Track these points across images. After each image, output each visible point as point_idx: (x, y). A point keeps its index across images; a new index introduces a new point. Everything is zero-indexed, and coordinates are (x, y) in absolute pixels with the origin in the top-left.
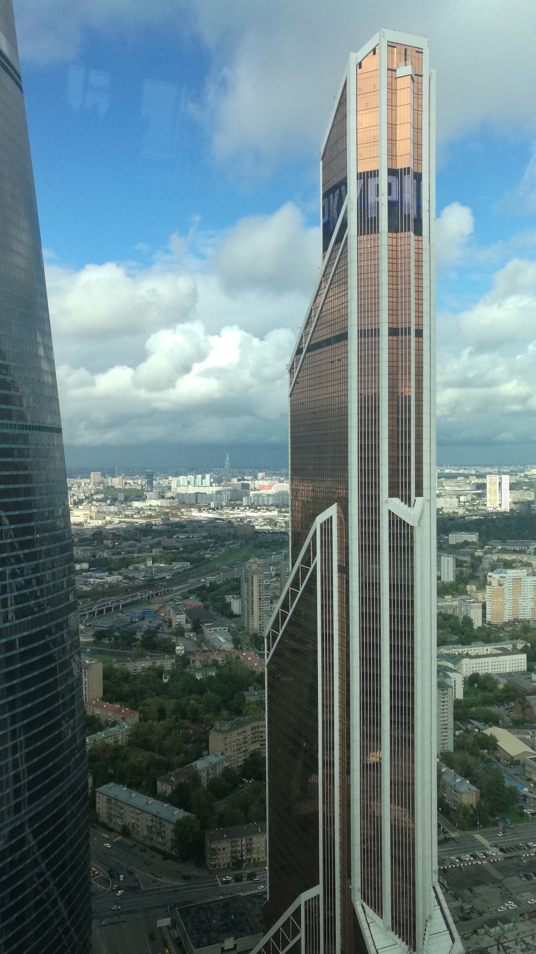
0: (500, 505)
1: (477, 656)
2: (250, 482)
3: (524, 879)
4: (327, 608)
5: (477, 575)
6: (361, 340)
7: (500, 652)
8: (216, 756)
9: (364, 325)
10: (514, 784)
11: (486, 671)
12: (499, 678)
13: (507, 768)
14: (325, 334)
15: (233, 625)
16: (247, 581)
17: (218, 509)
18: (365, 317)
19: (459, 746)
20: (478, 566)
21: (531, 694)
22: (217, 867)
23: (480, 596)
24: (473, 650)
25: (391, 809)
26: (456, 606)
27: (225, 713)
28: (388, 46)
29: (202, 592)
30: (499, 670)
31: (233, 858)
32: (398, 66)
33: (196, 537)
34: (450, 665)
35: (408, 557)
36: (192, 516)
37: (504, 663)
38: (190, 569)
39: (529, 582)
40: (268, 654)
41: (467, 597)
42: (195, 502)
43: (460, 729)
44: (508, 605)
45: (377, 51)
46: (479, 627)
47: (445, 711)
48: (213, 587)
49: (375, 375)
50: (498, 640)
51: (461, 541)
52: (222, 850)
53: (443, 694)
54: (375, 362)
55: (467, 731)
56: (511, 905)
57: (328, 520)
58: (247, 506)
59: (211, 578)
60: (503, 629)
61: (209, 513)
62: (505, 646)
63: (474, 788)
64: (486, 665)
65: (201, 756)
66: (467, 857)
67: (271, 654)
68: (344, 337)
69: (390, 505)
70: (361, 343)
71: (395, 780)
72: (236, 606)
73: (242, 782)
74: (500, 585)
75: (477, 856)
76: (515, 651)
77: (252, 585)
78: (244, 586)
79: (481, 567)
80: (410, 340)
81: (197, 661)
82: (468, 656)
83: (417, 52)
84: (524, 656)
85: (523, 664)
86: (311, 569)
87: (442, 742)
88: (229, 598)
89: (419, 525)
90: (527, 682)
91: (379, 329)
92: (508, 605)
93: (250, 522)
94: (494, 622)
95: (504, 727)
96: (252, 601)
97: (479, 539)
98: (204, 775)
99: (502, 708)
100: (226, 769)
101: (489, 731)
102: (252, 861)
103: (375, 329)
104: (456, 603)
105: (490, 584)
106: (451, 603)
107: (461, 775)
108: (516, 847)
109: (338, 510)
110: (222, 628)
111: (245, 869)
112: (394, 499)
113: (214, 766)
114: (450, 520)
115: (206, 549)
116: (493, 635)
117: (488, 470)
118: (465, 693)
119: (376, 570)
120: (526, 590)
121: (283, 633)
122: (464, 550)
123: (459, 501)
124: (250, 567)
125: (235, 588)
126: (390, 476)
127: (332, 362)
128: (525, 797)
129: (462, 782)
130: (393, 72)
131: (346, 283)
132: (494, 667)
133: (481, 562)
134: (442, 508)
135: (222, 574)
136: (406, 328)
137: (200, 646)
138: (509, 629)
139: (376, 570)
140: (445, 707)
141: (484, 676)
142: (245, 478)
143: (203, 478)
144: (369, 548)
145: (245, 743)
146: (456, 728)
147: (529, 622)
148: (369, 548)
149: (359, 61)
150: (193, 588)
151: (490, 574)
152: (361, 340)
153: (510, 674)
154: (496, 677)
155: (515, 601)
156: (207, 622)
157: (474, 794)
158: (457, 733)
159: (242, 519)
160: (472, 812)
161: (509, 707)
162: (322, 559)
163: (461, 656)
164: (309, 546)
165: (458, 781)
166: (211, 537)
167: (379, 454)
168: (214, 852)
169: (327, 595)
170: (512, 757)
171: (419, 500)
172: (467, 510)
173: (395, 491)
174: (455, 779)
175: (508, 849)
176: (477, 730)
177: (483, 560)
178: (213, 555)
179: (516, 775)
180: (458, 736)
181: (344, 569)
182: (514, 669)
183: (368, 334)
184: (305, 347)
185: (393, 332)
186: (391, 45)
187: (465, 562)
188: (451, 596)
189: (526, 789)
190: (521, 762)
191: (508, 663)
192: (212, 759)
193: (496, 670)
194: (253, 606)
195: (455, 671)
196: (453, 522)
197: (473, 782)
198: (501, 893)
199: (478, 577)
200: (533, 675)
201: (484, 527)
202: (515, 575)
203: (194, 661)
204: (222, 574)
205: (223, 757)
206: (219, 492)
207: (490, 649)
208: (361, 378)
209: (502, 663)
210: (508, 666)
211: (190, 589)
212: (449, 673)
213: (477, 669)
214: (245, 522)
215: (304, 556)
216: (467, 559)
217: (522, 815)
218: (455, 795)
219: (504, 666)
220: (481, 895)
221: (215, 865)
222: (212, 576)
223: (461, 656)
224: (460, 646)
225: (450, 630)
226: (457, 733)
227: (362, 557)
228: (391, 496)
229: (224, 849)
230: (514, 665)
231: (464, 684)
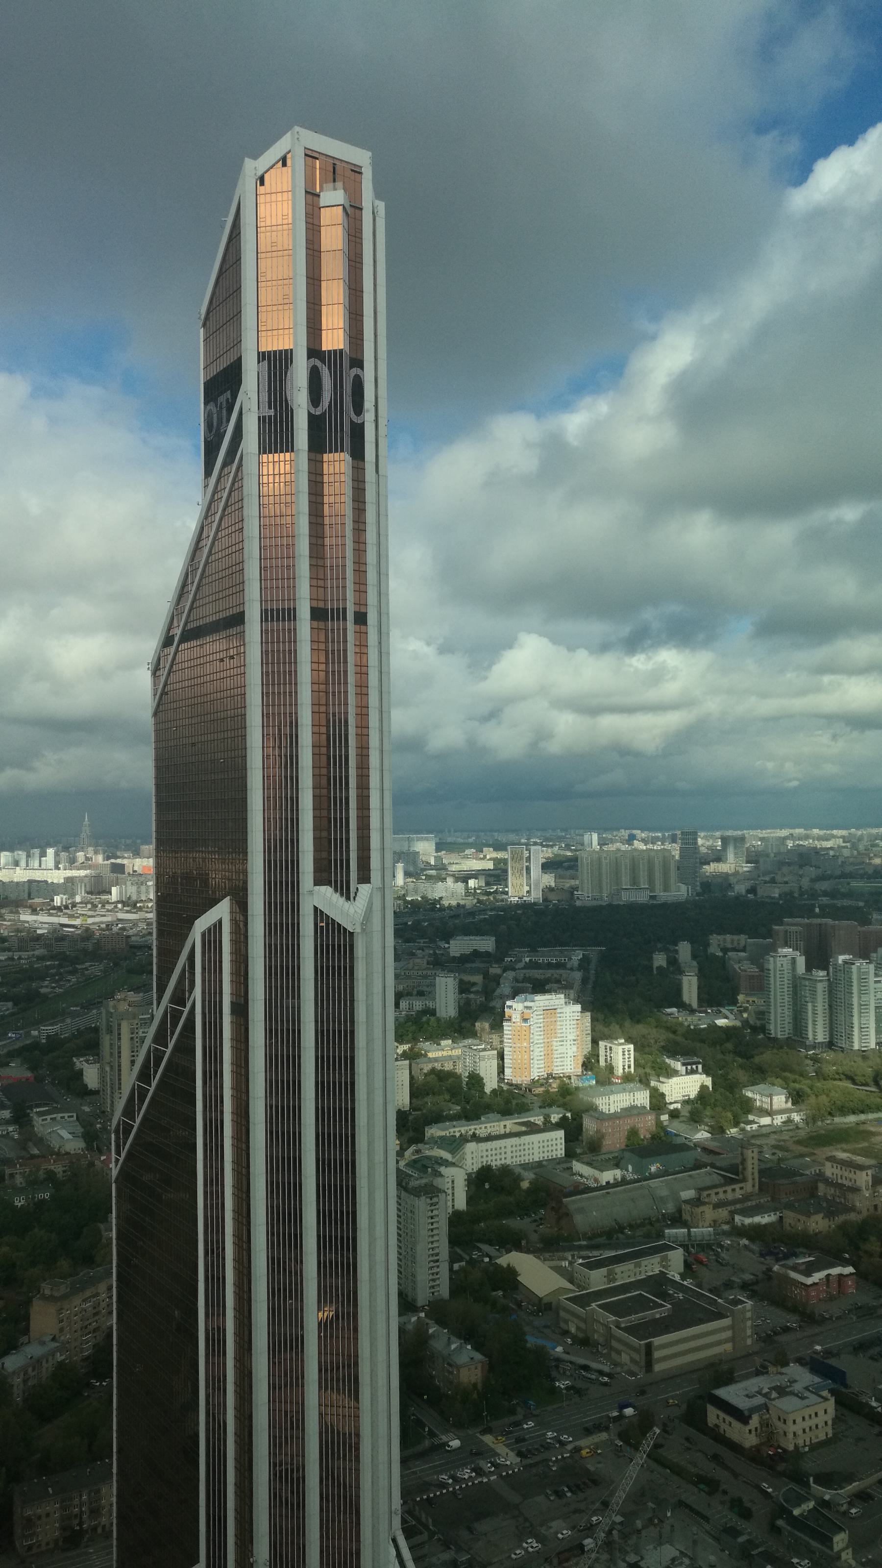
0: (528, 892)
1: (489, 1138)
2: (125, 862)
3: (552, 1498)
4: (213, 1075)
5: (492, 1004)
6: (267, 626)
7: (524, 1129)
8: (43, 1343)
9: (272, 601)
10: (540, 1342)
11: (503, 1162)
12: (522, 1172)
13: (531, 1318)
14: (209, 613)
15: (86, 1109)
16: (110, 1031)
17: (66, 907)
18: (283, 587)
19: (458, 1287)
20: (494, 991)
21: (571, 1194)
22: (35, 1550)
23: (495, 1038)
24: (483, 1128)
25: (320, 1414)
26: (458, 1057)
27: (64, 1264)
28: (306, 155)
29: (30, 1053)
30: (522, 1158)
31: (63, 1529)
32: (321, 189)
33: (24, 957)
34: (446, 1155)
36: (19, 921)
38: (13, 1014)
39: (568, 1015)
40: (117, 1161)
41: (477, 1041)
42: (26, 896)
43: (460, 1259)
44: (538, 1052)
45: (289, 162)
46: (494, 1091)
47: (435, 1232)
48: (54, 1042)
49: (290, 684)
50: (523, 1109)
51: (468, 951)
53: (432, 1205)
54: (290, 663)
55: (471, 1262)
56: (532, 1545)
57: (215, 925)
58: (118, 902)
59: (49, 1029)
60: (530, 1091)
61: (51, 915)
62: (532, 1119)
63: (478, 1356)
64: (503, 1150)
65: (15, 1347)
66: (466, 1473)
67: (121, 1159)
68: (239, 619)
69: (318, 897)
70: (267, 630)
71: (326, 1362)
72: (91, 1076)
73: (88, 1385)
74: (525, 1020)
75: (481, 1469)
76: (549, 1126)
77: (119, 1039)
78: (106, 1040)
79: (498, 992)
80: (345, 630)
81: (17, 1176)
82: (475, 1138)
83: (352, 170)
84: (561, 1134)
85: (559, 1147)
86: (186, 1010)
87: (432, 1284)
88: (79, 1063)
89: (363, 930)
90: (566, 1175)
91: (295, 609)
92: (538, 1052)
93: (123, 929)
94: (517, 1080)
95: (528, 1252)
96: (119, 1066)
97: (497, 947)
98: (18, 1381)
99: (527, 1220)
100: (61, 1364)
101: (504, 1260)
102: (100, 1530)
103: (289, 609)
104: (457, 1052)
106: (450, 1053)
107: (459, 1336)
108: (542, 1446)
109: (231, 908)
110: (66, 1115)
111: (87, 1547)
112: (323, 888)
113: (37, 1363)
114: (452, 917)
115: (43, 979)
116: (514, 1102)
117: (512, 837)
118: (470, 1200)
119: (293, 1008)
120: (564, 1027)
121: (142, 1123)
122: (474, 965)
123: (467, 888)
124: (115, 1007)
125: (90, 1044)
126: (315, 851)
127: (222, 660)
128: (558, 1360)
129: (460, 1348)
130: (315, 198)
131: (241, 529)
132: (514, 1154)
133: (498, 984)
134: (441, 898)
135: (69, 1021)
136: (338, 609)
137: (25, 1149)
138: (540, 1090)
139: (293, 1008)
140: (435, 1225)
141: (499, 1170)
142: (119, 854)
143: (43, 854)
144: (283, 973)
145: (95, 1314)
146: (454, 1258)
147: (569, 1077)
148: (283, 973)
149: (260, 173)
150: (16, 1047)
151: (508, 1003)
152: (267, 626)
153: (540, 1164)
154: (518, 1170)
155: (548, 1046)
156: (38, 1106)
157: (479, 1366)
158: (456, 1266)
159: (109, 926)
160: (475, 1396)
161: (537, 1218)
162: (203, 992)
163: (464, 1140)
164: (184, 970)
165: (453, 1347)
166: (52, 958)
167: (297, 814)
168: (29, 1522)
169: (213, 1055)
170: (540, 1299)
171: (365, 889)
172: (479, 901)
173: (325, 875)
174: (449, 1343)
175: (529, 1451)
176: (487, 1260)
177: (502, 981)
178: (54, 988)
179: (546, 1327)
180: (457, 1272)
181: (241, 1010)
183: (279, 615)
184: (177, 632)
185: (318, 614)
186: (311, 155)
187: (474, 984)
188: (450, 1041)
189: (559, 1349)
190: (554, 1306)
191: (536, 1145)
192: (33, 1350)
193: (518, 1159)
194: (120, 1075)
195: (453, 1164)
196: (457, 921)
197: (477, 1348)
198: (517, 1527)
199: (493, 1008)
200: (574, 1162)
201: (503, 927)
202: (547, 1003)
203: (12, 1176)
204: (69, 1021)
205: (55, 1345)
206: (69, 880)
207: (509, 1124)
208: (268, 688)
209: (526, 1147)
210: (536, 1151)
211: (11, 1048)
212: (443, 1170)
213: (489, 1158)
214: (115, 929)
215: (176, 988)
216: (478, 979)
217: (554, 1391)
218: (449, 1372)
219: (531, 1151)
220: (485, 1534)
221: (30, 1548)
222: (52, 1025)
223: (464, 1140)
224: (463, 1122)
225: (447, 1097)
226: (456, 1266)
227: (270, 987)
228: (317, 883)
229: (48, 1515)
230: (546, 1149)
231: (468, 1186)
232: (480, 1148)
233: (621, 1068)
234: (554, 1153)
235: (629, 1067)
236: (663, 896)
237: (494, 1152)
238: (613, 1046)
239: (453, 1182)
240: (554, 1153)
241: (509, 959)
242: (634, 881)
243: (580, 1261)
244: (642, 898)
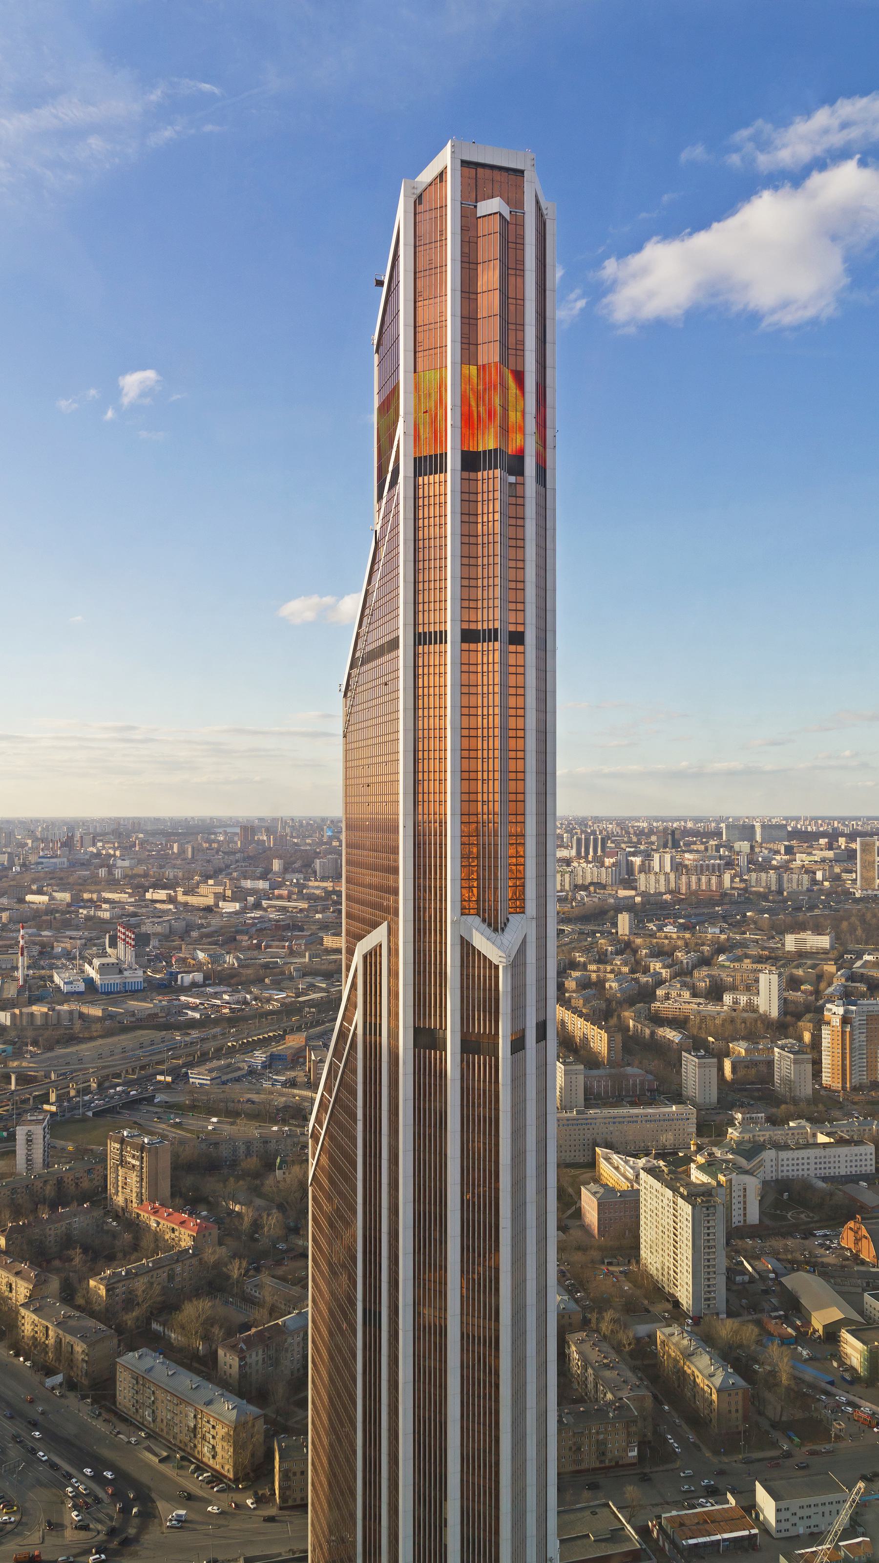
30: (827, 1171)
35: (371, 1038)
37: (837, 1159)
52: (298, 1474)
64: (805, 1161)
85: (869, 1162)
86: (352, 1029)
105: (828, 1023)
112: (470, 919)
132: (818, 1166)
182: (854, 1170)
209: (832, 1160)
210: (843, 1166)
219: (837, 1165)
230: (853, 1164)
239: (745, 1189)
240: (837, 1171)
241: (849, 956)
243: (668, 1241)
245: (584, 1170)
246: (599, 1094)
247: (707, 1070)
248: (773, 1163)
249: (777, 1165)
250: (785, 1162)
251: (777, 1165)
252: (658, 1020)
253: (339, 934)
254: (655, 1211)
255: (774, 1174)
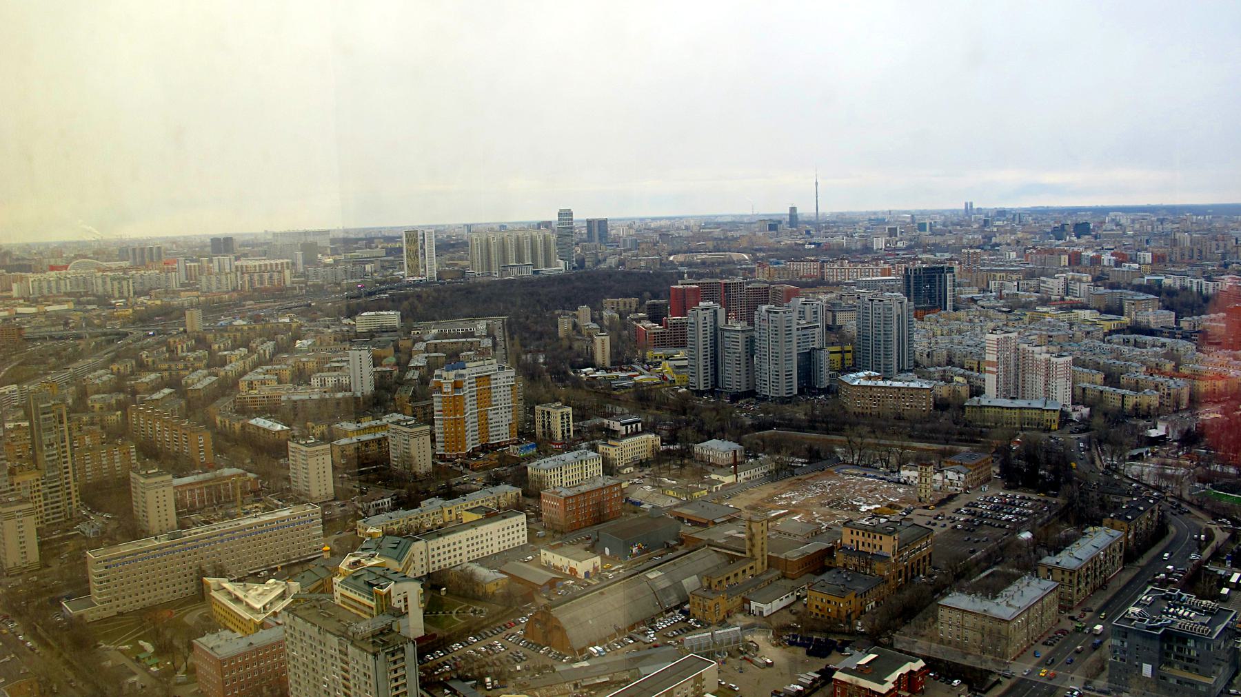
30: (480, 552)
209: (484, 538)
210: (495, 542)
219: (489, 543)
230: (506, 538)
232: (430, 547)
233: (560, 433)
234: (516, 540)
235: (569, 431)
236: (545, 271)
237: (447, 549)
238: (552, 411)
239: (406, 599)
242: (520, 258)
244: (527, 273)
245: (189, 608)
246: (193, 504)
247: (320, 458)
248: (423, 556)
249: (427, 557)
250: (436, 552)
251: (427, 557)
252: (244, 410)
253: (402, 269)
254: (311, 666)
255: (424, 569)
